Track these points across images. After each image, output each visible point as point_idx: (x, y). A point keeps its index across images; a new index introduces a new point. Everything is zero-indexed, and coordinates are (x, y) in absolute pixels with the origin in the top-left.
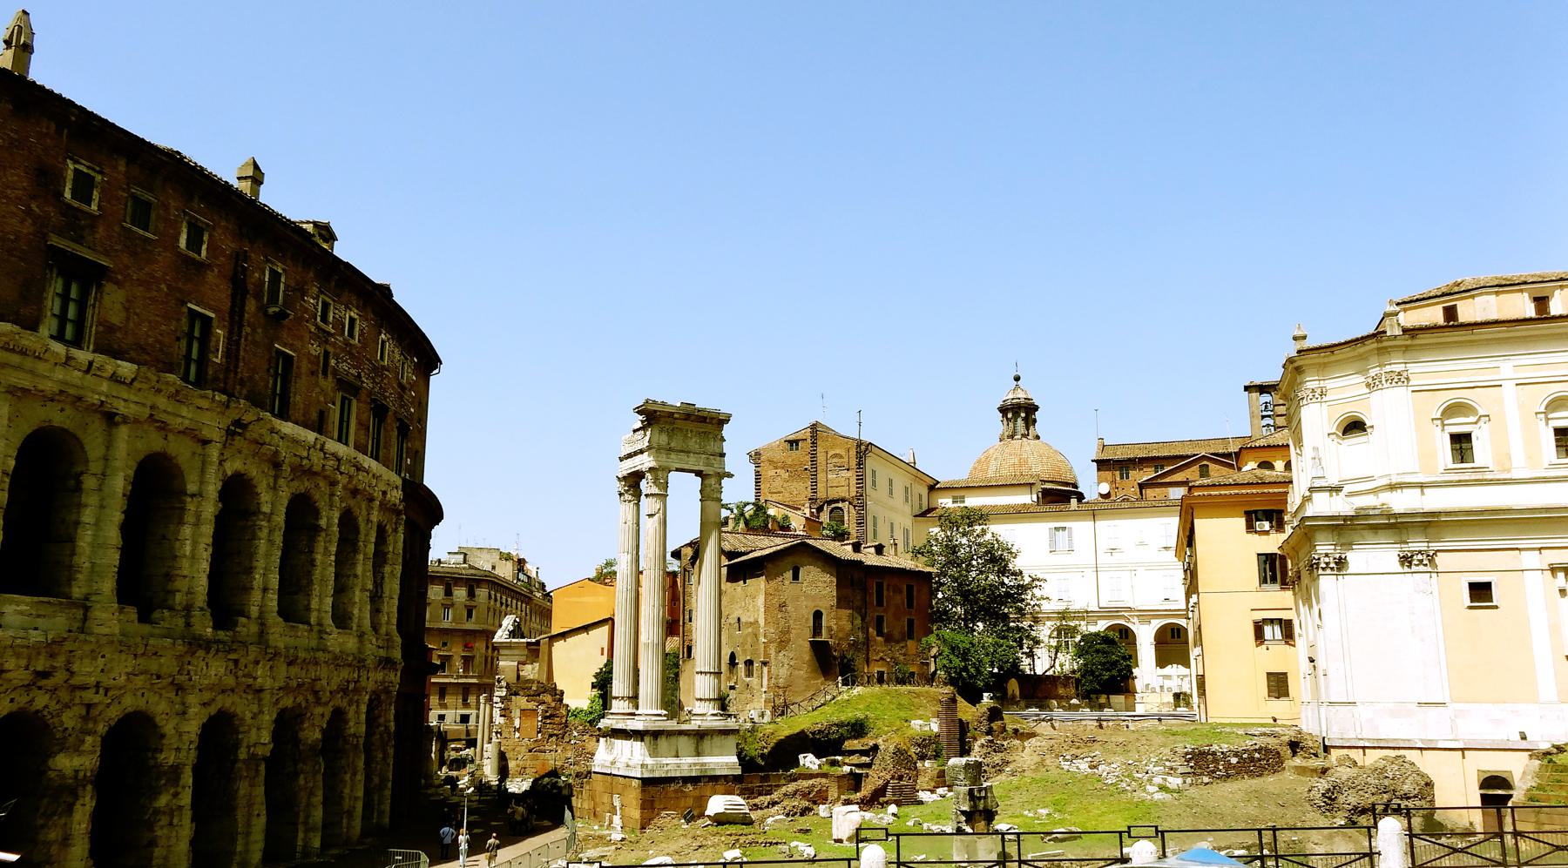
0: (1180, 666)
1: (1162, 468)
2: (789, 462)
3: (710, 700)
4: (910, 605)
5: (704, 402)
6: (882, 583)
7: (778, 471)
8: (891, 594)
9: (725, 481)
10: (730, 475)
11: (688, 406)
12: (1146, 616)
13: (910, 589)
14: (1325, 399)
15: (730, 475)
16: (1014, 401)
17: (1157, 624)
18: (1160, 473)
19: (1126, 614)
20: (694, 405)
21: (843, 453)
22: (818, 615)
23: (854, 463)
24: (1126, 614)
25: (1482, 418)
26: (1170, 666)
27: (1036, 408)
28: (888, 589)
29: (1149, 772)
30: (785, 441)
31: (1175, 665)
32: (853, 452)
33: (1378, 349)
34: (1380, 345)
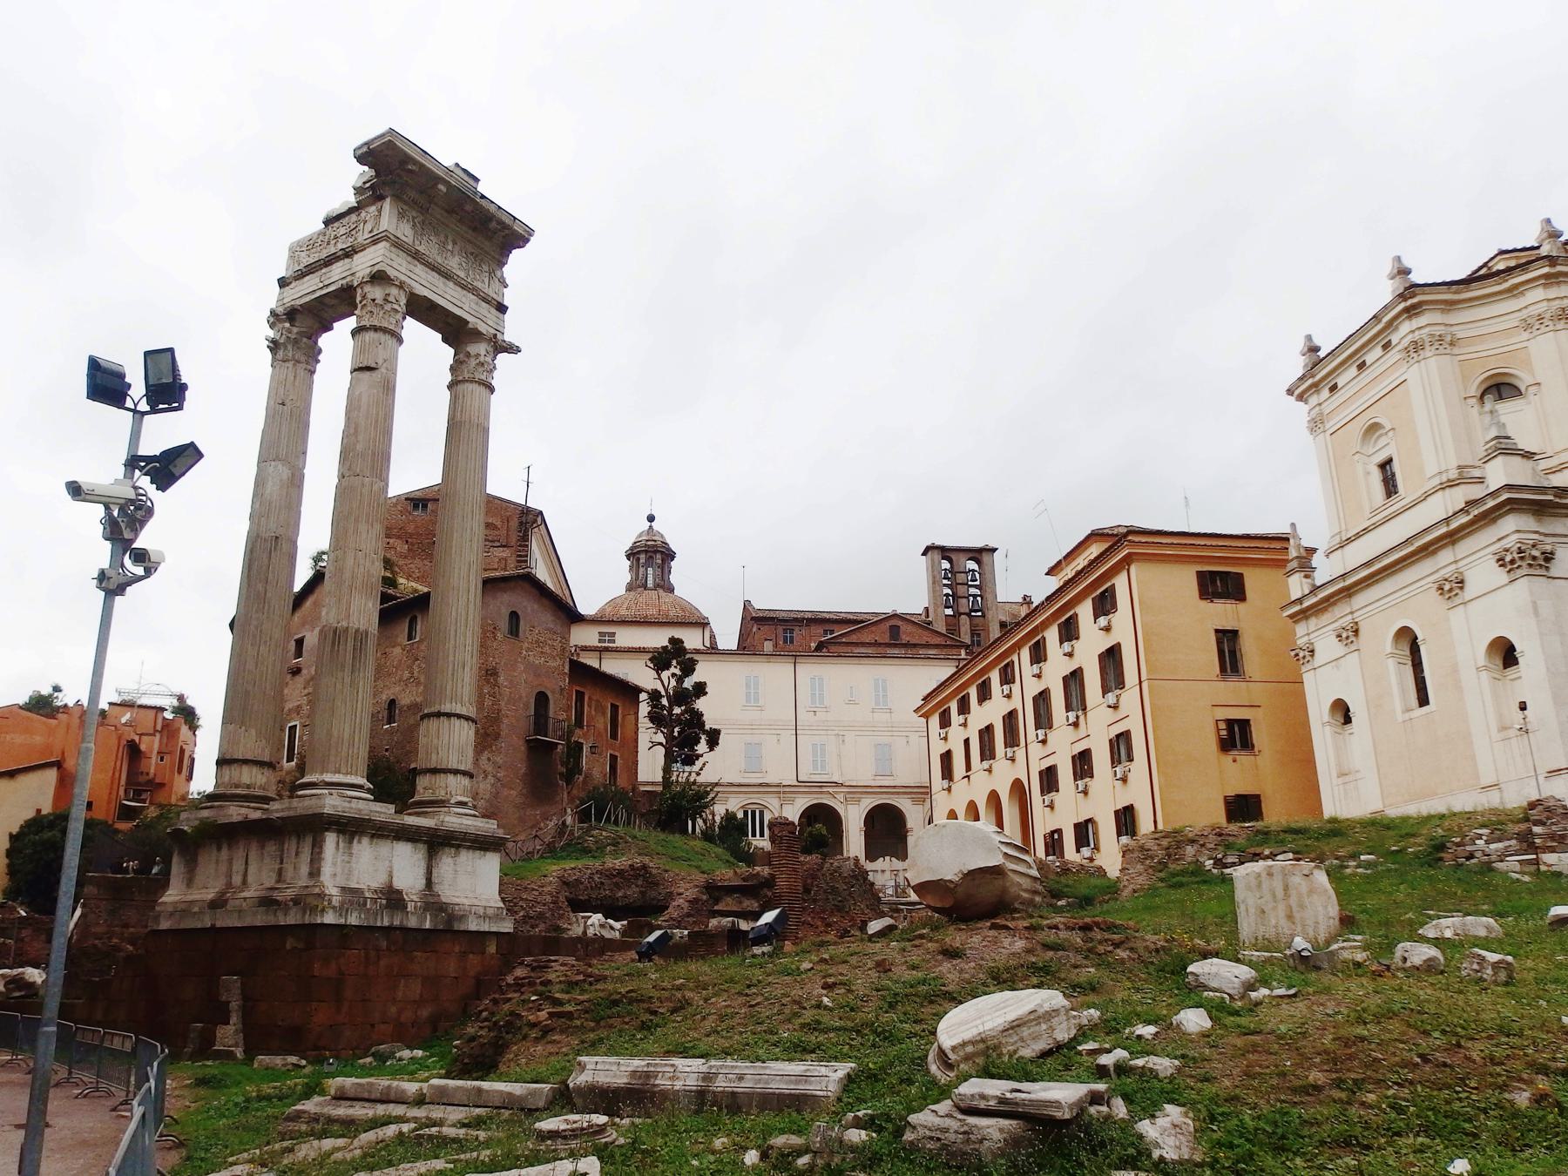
0: (893, 859)
1: (832, 632)
2: (411, 529)
3: (435, 771)
4: (614, 736)
5: (498, 189)
6: (583, 693)
7: (391, 541)
8: (593, 713)
9: (502, 358)
10: (512, 349)
11: (466, 178)
12: (855, 792)
13: (615, 708)
14: (1456, 351)
15: (512, 349)
16: (649, 543)
17: (868, 803)
18: (829, 637)
19: (831, 790)
20: (477, 180)
21: (498, 524)
22: (542, 699)
23: (513, 540)
24: (831, 790)
25: (1530, 388)
26: (882, 859)
27: (673, 558)
28: (590, 706)
29: (1478, 854)
30: (406, 499)
31: (887, 858)
32: (514, 523)
33: (1546, 276)
34: (1553, 270)
